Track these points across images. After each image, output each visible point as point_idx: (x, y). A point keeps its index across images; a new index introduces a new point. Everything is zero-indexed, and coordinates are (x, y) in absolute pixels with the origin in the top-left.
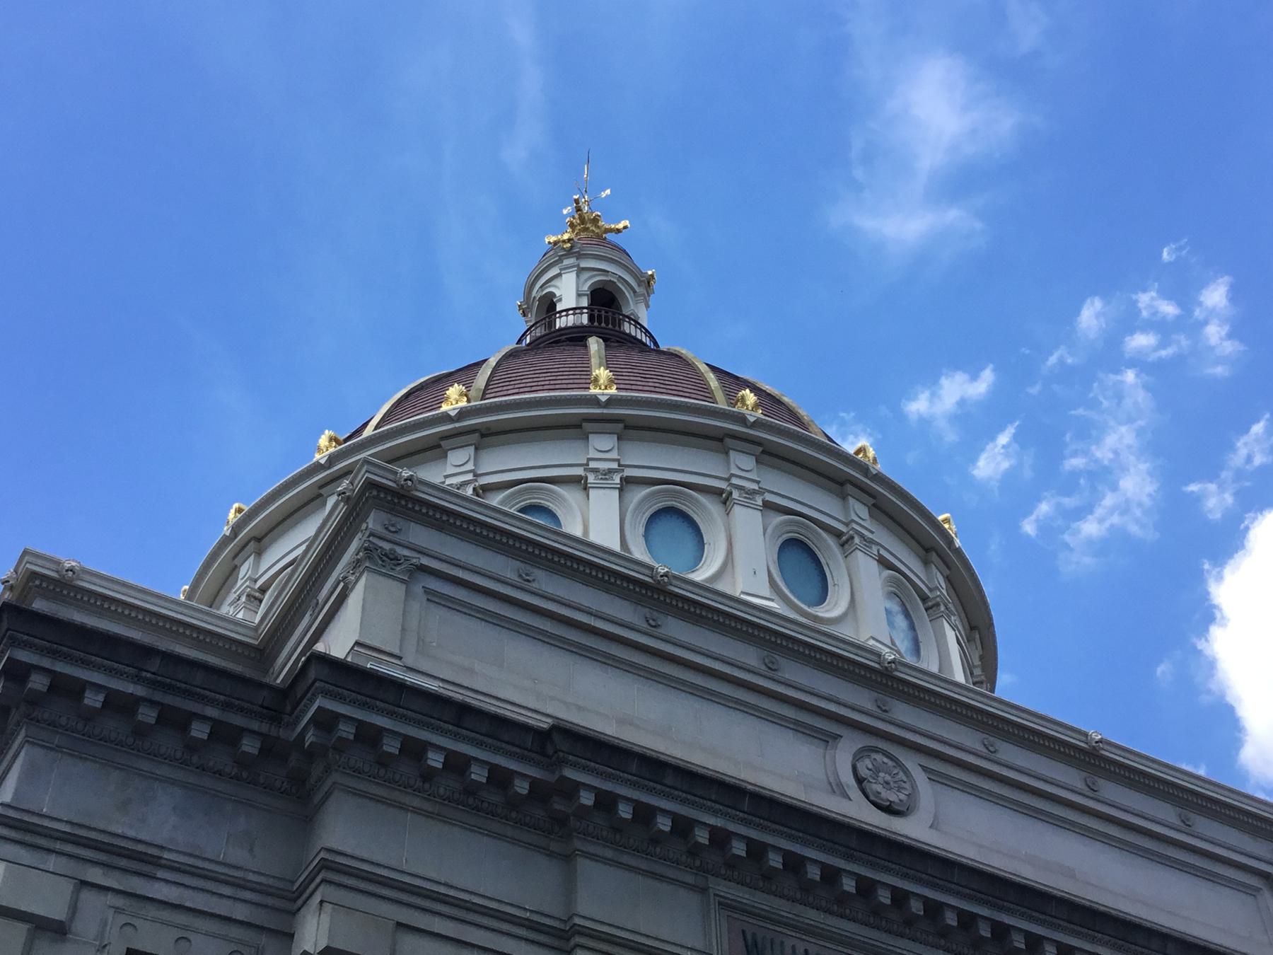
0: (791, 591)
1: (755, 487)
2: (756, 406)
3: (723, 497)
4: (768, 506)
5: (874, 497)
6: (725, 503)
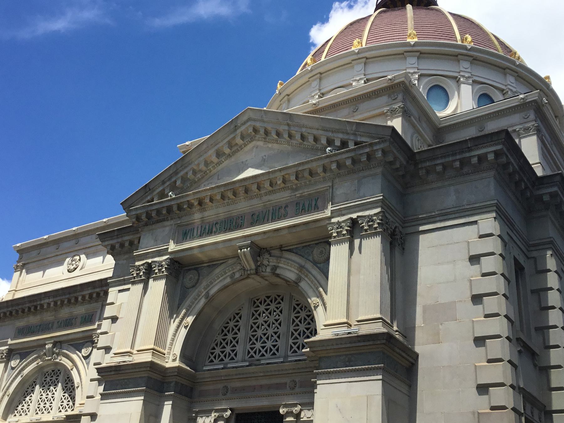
0: (450, 23)
1: (470, 75)
2: (472, 41)
3: (456, 80)
4: (474, 82)
5: (517, 73)
6: (457, 82)
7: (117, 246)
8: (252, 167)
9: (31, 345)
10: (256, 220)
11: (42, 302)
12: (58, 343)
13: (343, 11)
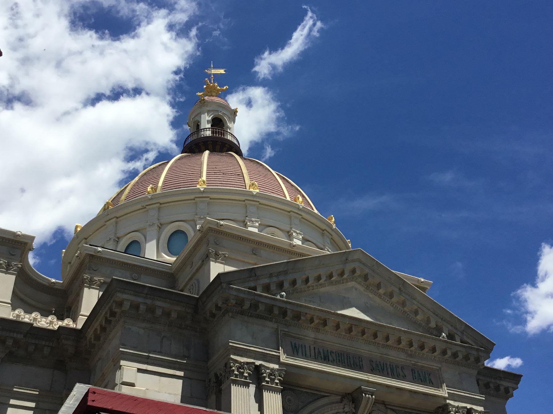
8: (358, 308)
13: (6, 28)
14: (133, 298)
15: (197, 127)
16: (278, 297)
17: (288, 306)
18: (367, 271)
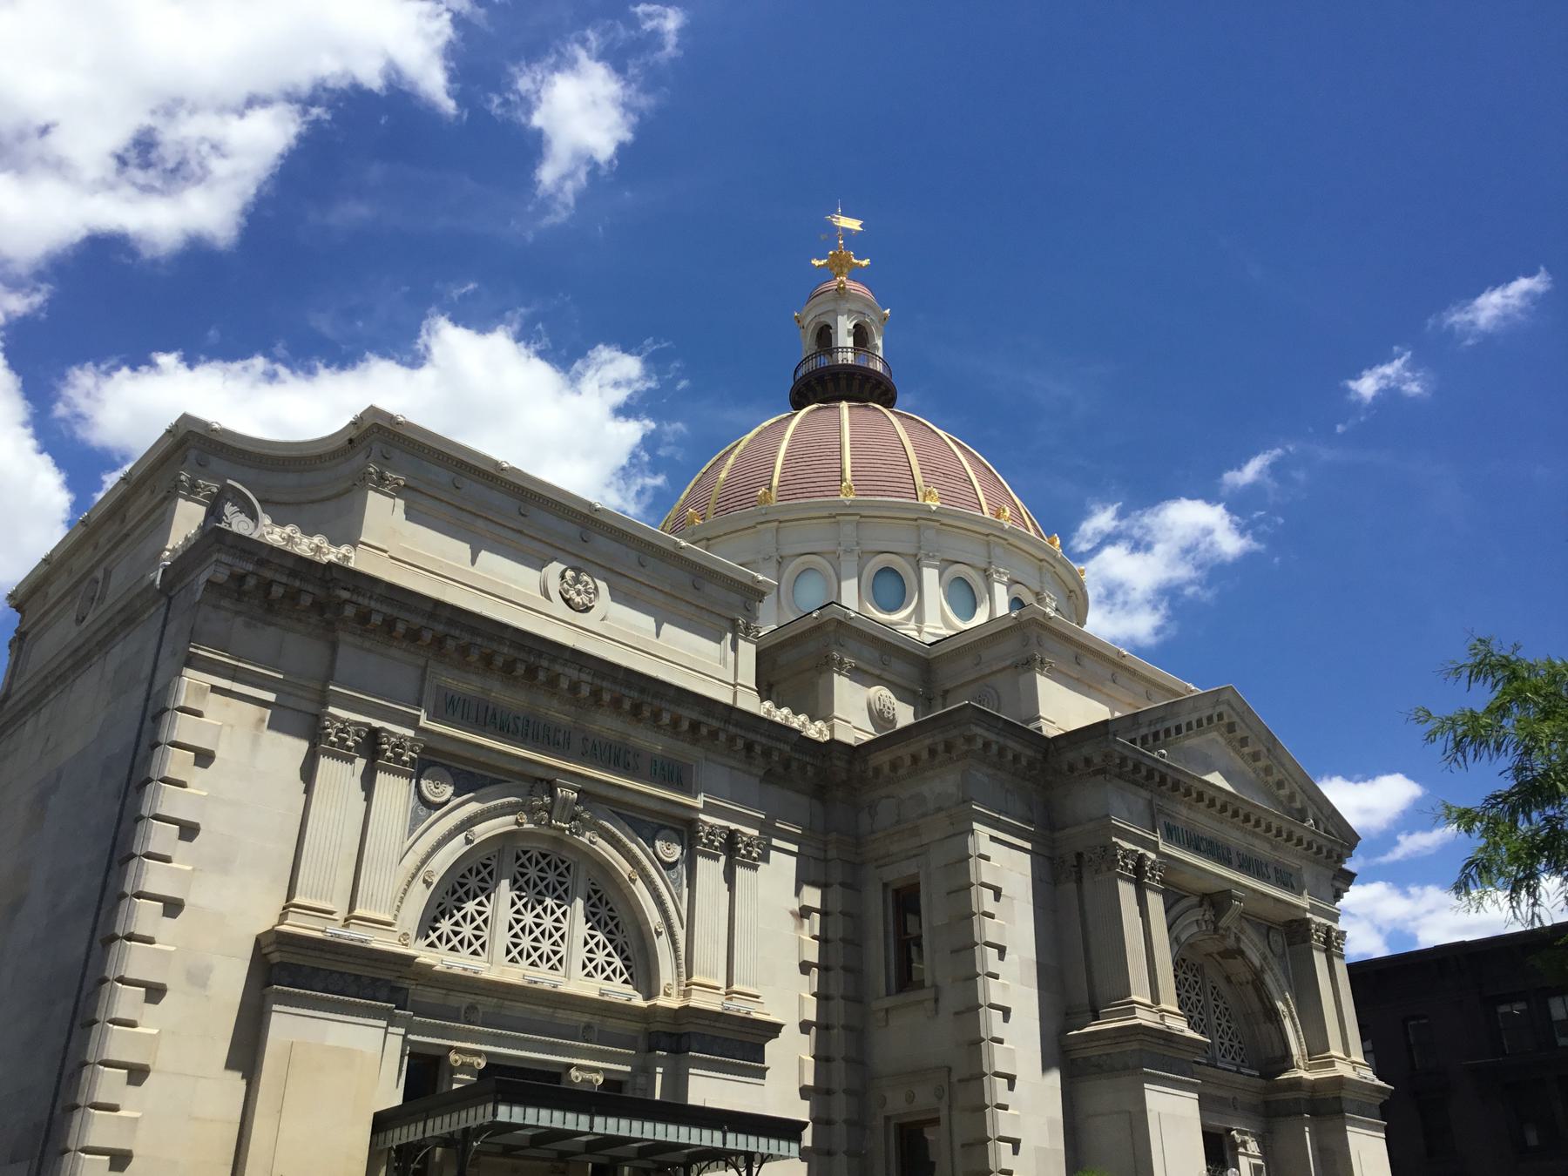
7: (995, 748)
9: (629, 798)
10: (1249, 865)
11: (558, 668)
12: (590, 795)
14: (986, 734)
15: (825, 335)
16: (1156, 755)
17: (1169, 772)
18: (1235, 719)
